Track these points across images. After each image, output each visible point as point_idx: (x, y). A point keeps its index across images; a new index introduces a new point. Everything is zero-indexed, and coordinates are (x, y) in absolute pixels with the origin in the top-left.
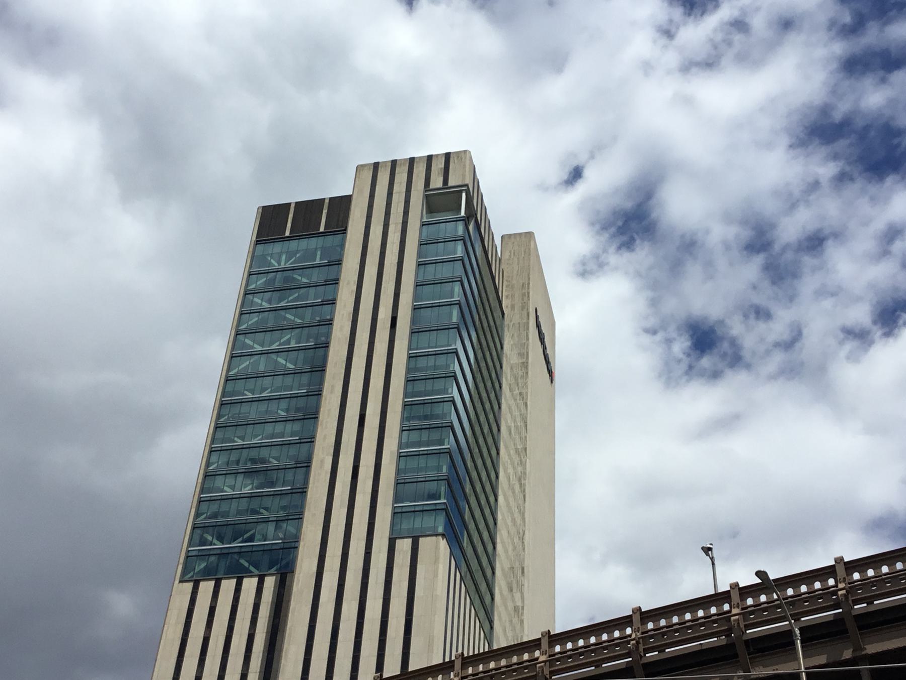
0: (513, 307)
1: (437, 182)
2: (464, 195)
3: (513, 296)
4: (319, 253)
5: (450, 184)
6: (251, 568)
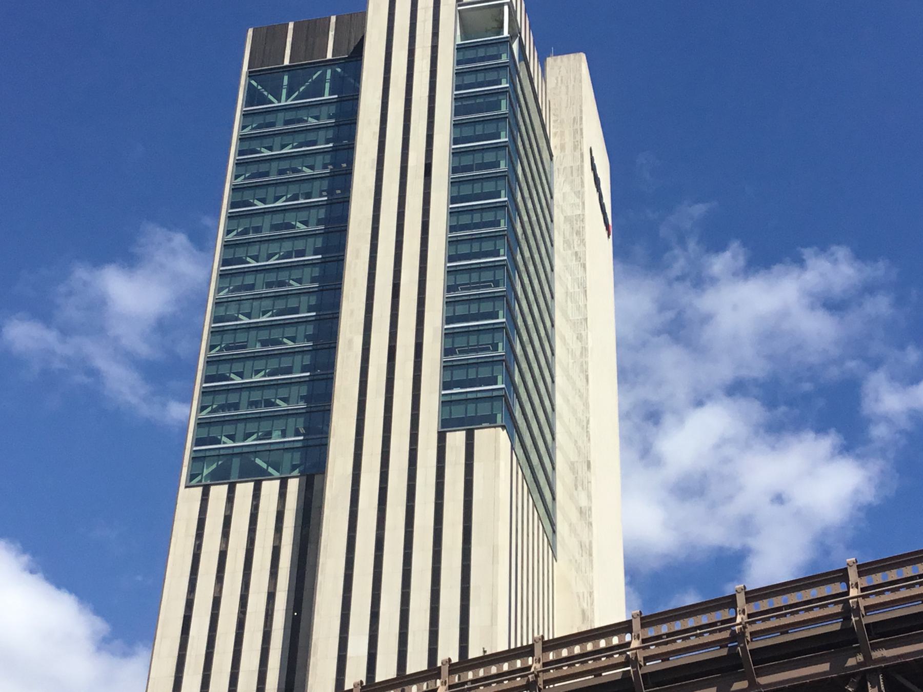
0: (563, 148)
2: (506, 8)
6: (271, 470)
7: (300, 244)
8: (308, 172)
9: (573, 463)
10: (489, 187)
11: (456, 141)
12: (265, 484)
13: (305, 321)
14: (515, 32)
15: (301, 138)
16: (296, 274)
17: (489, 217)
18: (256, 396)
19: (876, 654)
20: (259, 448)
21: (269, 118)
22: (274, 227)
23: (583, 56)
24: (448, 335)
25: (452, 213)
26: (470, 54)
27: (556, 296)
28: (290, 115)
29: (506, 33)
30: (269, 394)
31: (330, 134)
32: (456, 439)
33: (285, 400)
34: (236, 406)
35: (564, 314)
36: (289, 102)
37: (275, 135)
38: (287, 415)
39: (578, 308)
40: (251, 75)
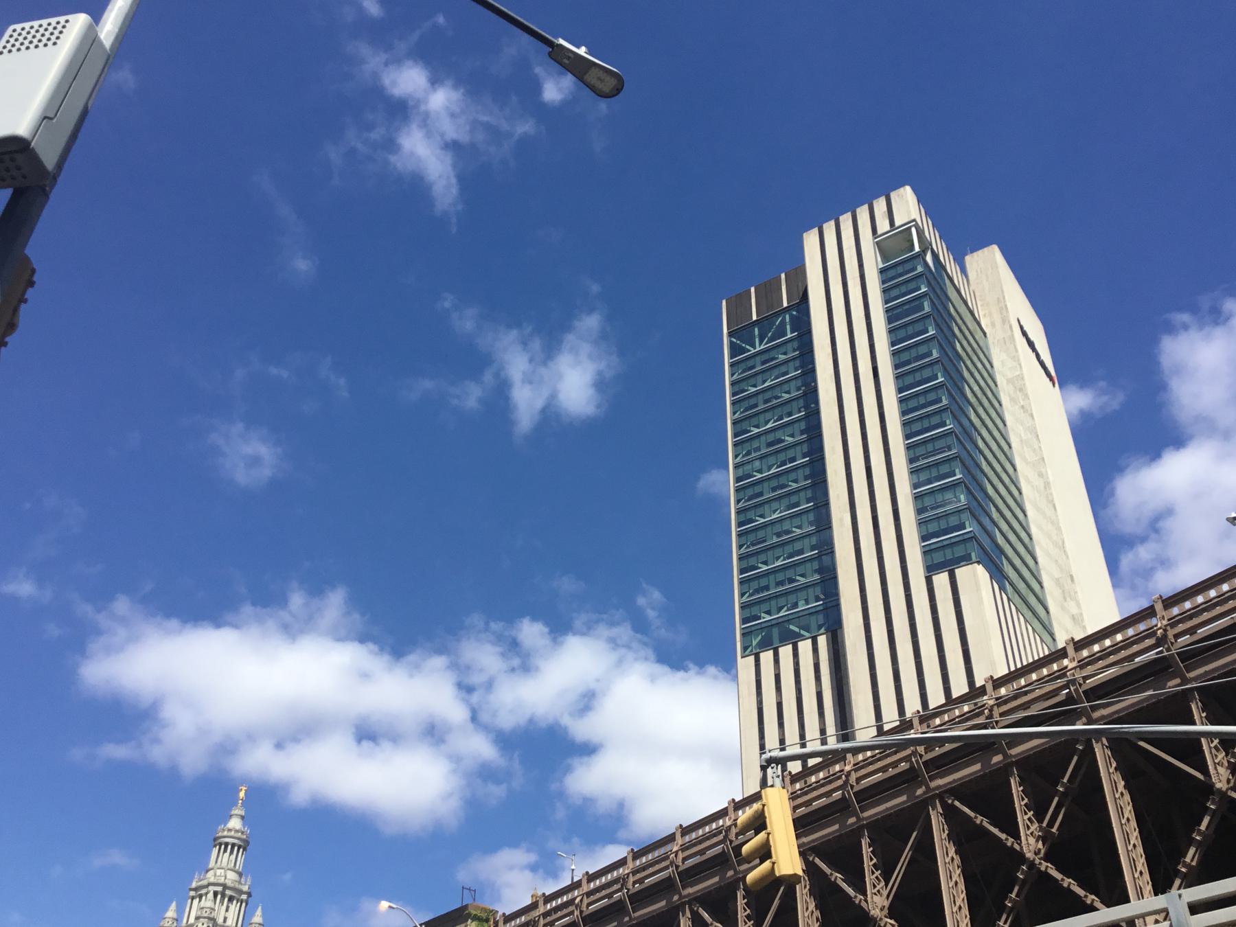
0: (993, 325)
1: (883, 226)
2: (914, 230)
3: (990, 314)
5: (897, 223)
6: (802, 632)
7: (790, 453)
8: (786, 396)
9: (1058, 580)
10: (927, 373)
11: (893, 344)
13: (806, 511)
14: (926, 246)
16: (793, 476)
17: (932, 396)
18: (780, 577)
19: (933, 784)
21: (750, 363)
22: (770, 444)
23: (995, 248)
24: (917, 498)
25: (901, 401)
26: (891, 273)
27: (1013, 445)
28: (764, 357)
29: (917, 249)
30: (790, 574)
31: (797, 363)
32: (941, 580)
33: (802, 575)
34: (767, 588)
35: (1024, 459)
36: (781, 614)
37: (756, 374)
38: (806, 587)
39: (1034, 450)
40: (730, 334)
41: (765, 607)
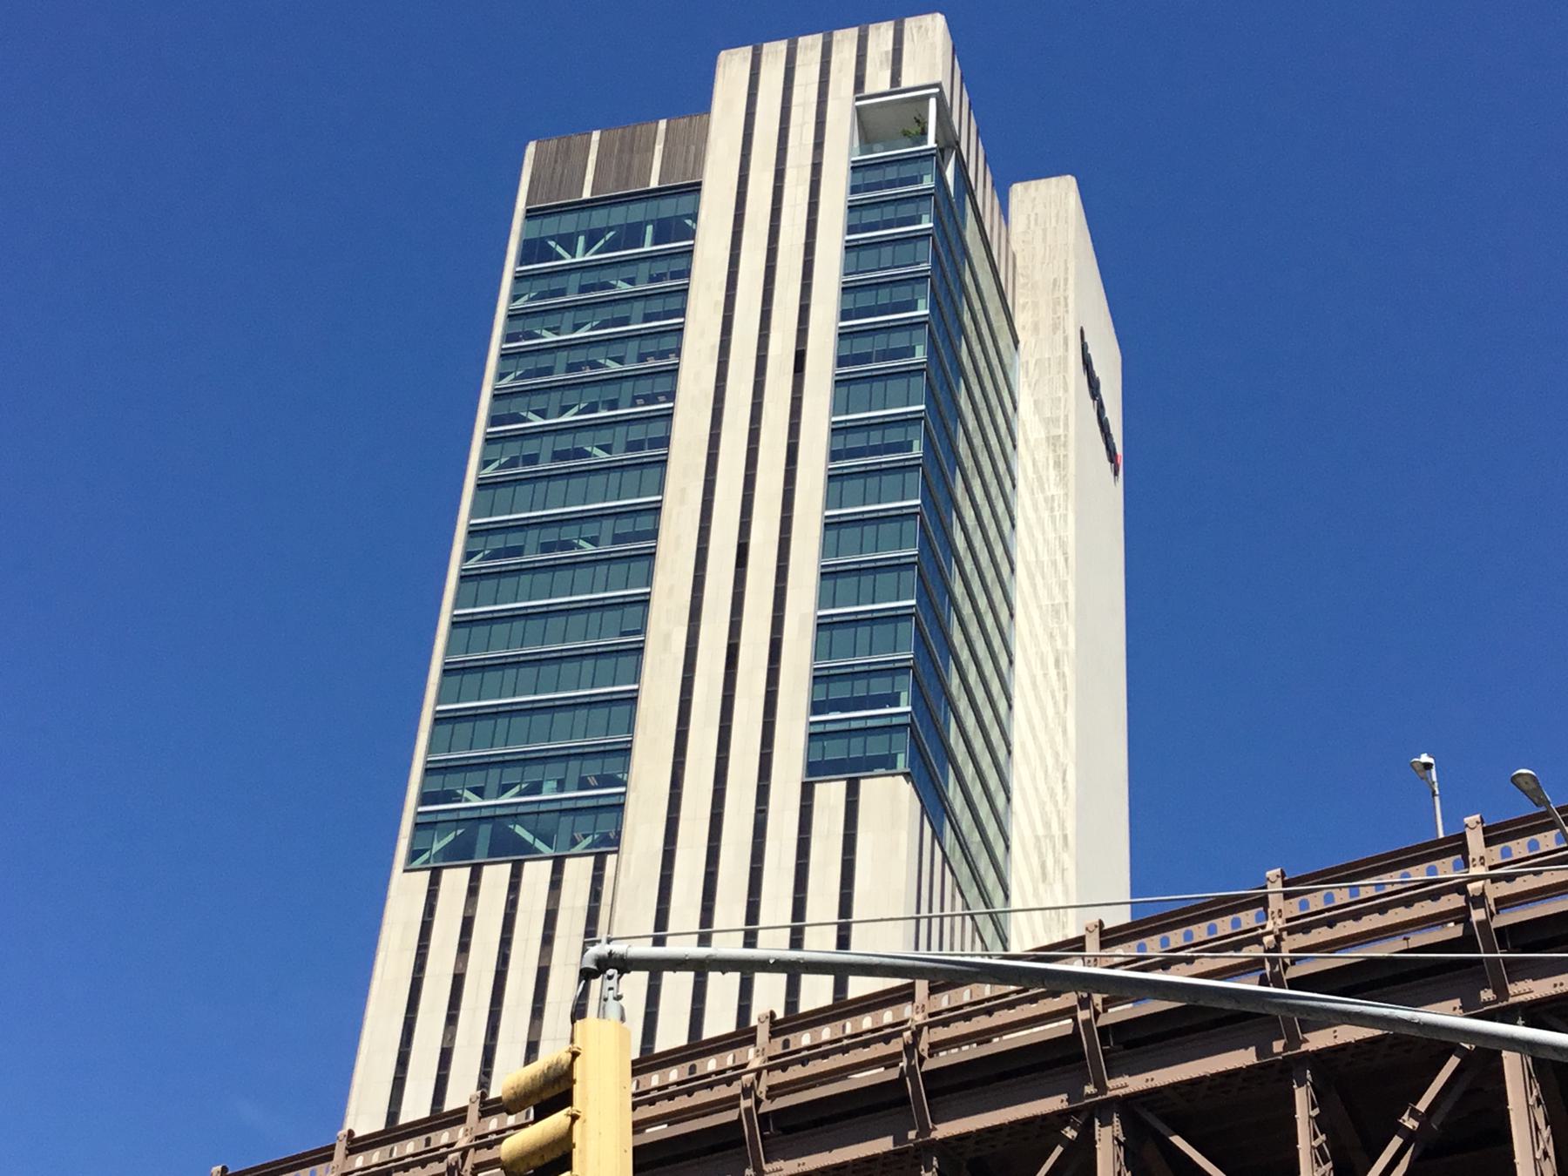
1: (878, 80)
4: (650, 229)
12: (529, 867)
15: (606, 313)
20: (521, 809)
41: (476, 778)
